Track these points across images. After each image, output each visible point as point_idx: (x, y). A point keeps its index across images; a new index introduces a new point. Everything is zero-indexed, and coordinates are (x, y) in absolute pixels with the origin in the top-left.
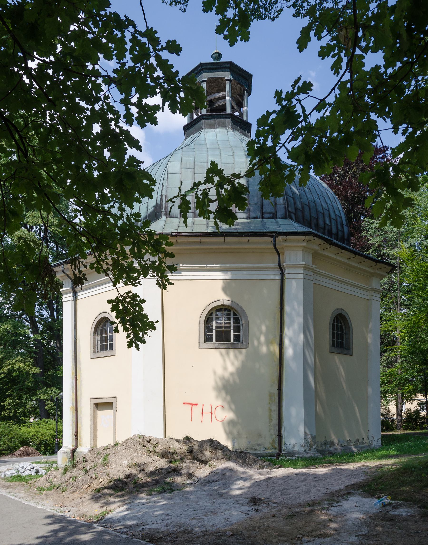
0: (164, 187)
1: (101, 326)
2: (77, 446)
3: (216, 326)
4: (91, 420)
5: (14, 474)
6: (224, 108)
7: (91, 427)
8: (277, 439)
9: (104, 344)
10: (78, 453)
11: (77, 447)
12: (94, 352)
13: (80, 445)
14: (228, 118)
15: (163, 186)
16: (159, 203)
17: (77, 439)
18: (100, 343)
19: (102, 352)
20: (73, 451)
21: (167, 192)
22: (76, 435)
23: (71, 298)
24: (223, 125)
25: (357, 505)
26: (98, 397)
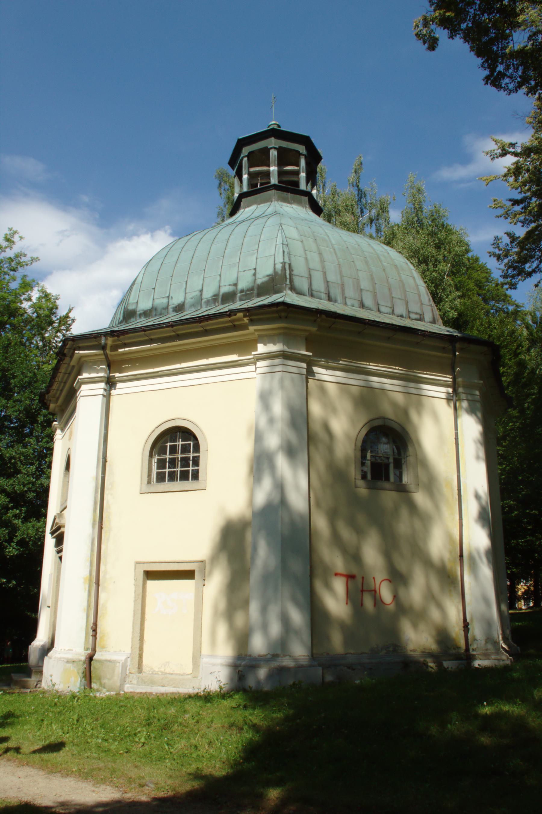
0: (286, 253)
1: (164, 439)
2: (94, 650)
3: (371, 456)
4: (135, 601)
5: (501, 663)
6: (296, 184)
7: (134, 615)
8: (463, 633)
9: (167, 470)
10: (99, 661)
11: (96, 651)
12: (149, 482)
13: (103, 647)
14: (305, 196)
15: (284, 252)
16: (280, 272)
17: (95, 636)
18: (158, 468)
19: (172, 483)
20: (90, 658)
21: (290, 259)
22: (95, 630)
23: (102, 392)
24: (299, 203)
25: (173, 768)
26: (157, 560)
